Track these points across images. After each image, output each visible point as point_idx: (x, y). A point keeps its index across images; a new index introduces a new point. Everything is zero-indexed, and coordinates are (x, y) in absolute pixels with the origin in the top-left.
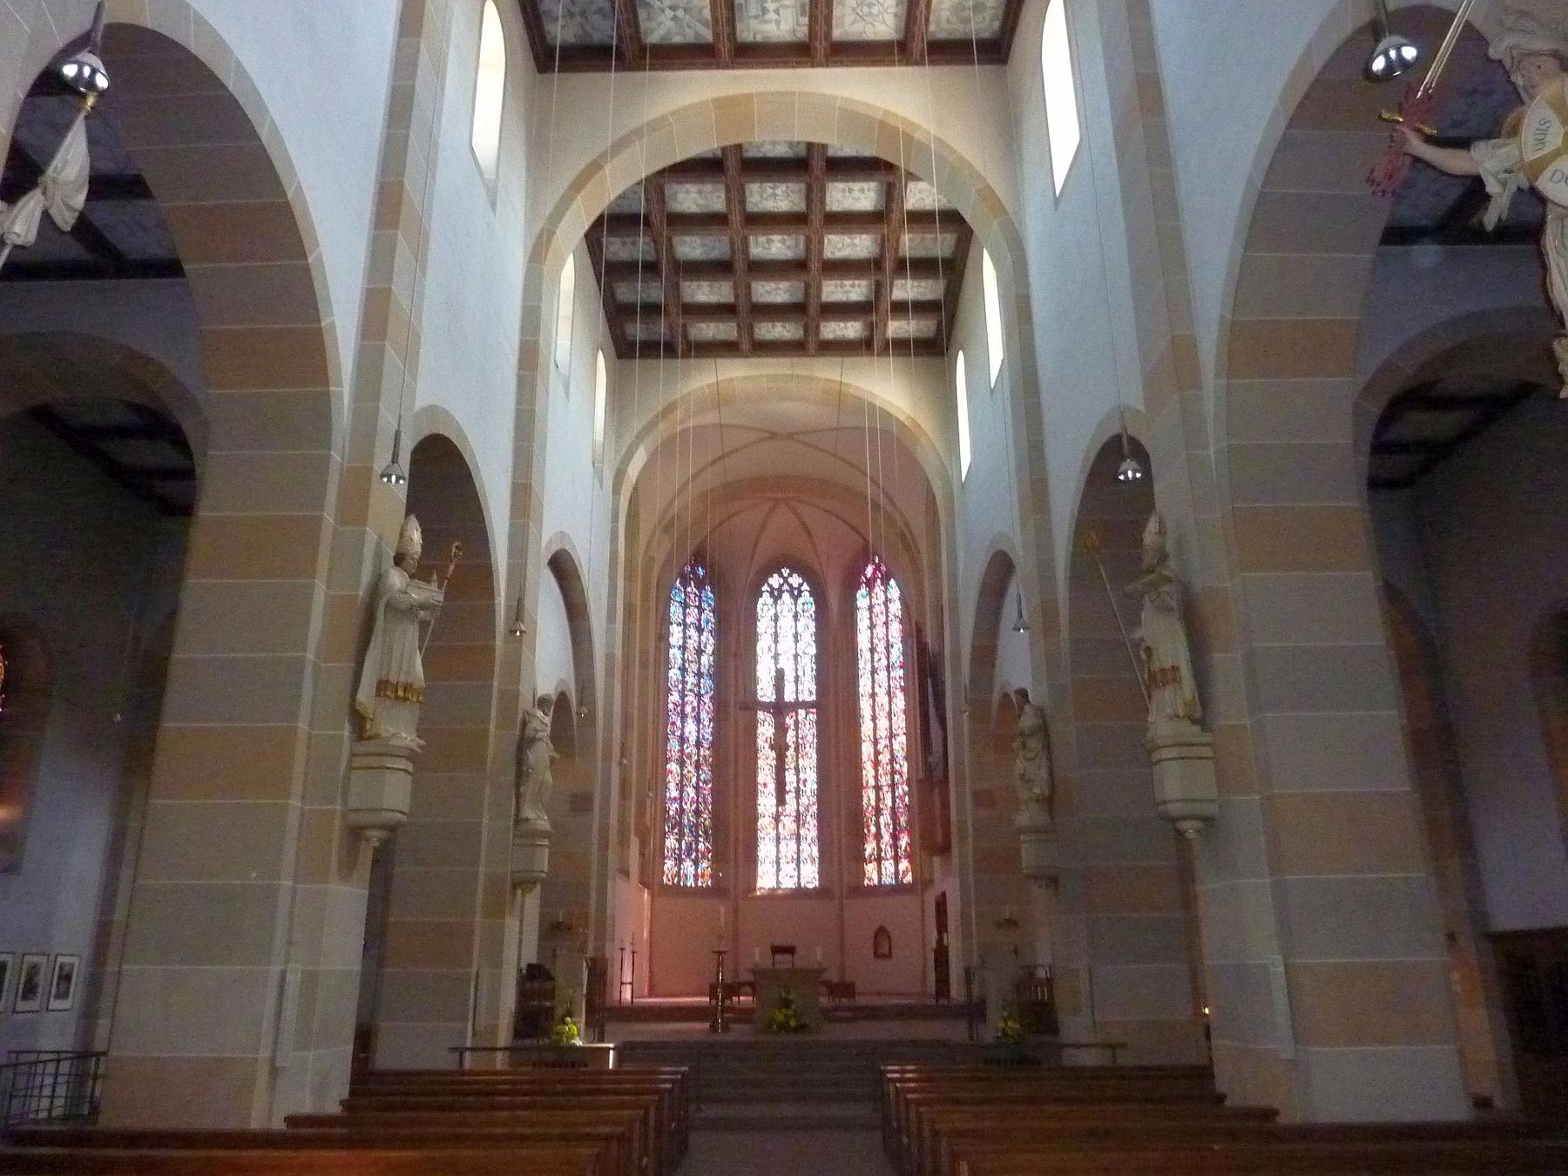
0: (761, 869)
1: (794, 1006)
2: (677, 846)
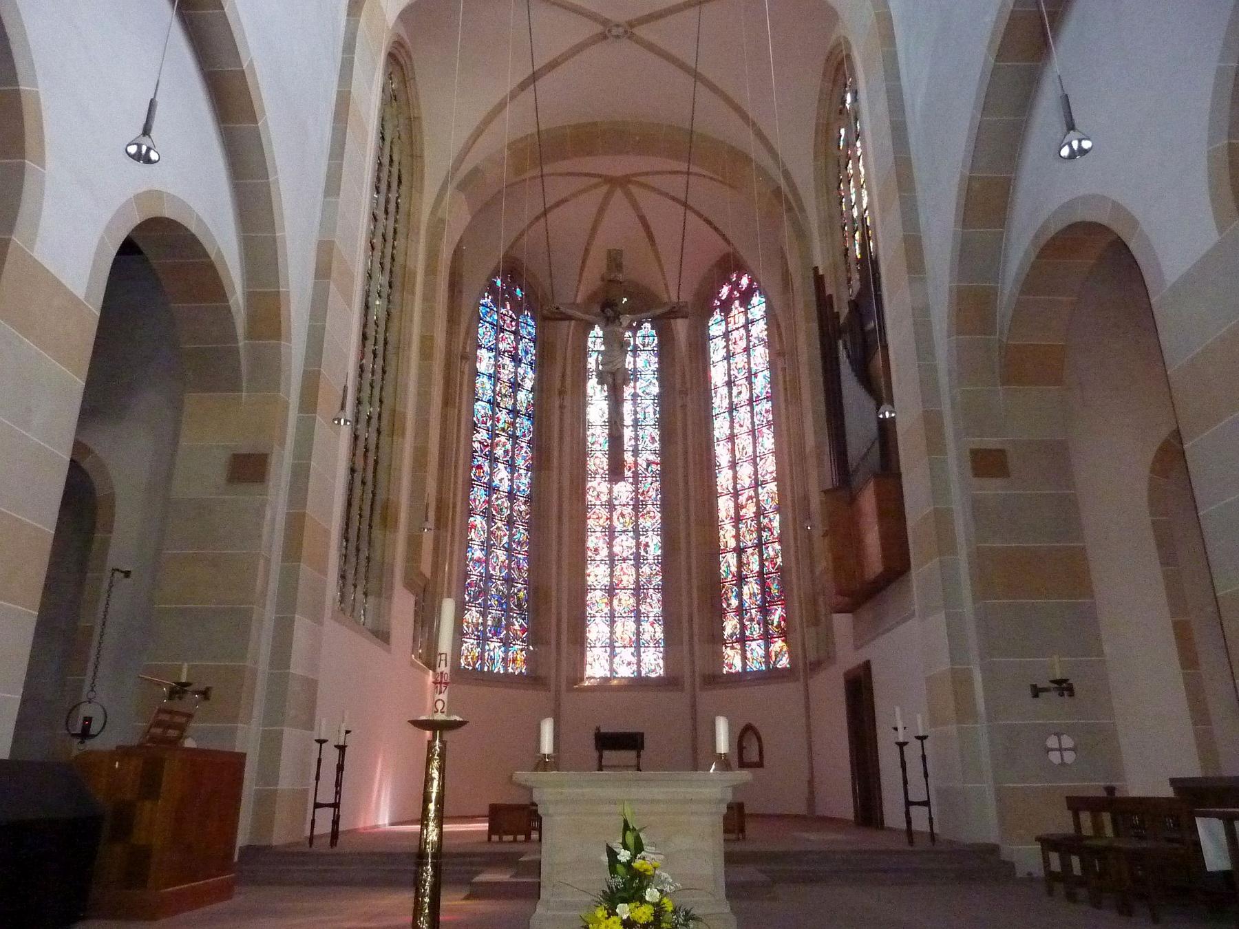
1: (651, 894)
2: (481, 621)
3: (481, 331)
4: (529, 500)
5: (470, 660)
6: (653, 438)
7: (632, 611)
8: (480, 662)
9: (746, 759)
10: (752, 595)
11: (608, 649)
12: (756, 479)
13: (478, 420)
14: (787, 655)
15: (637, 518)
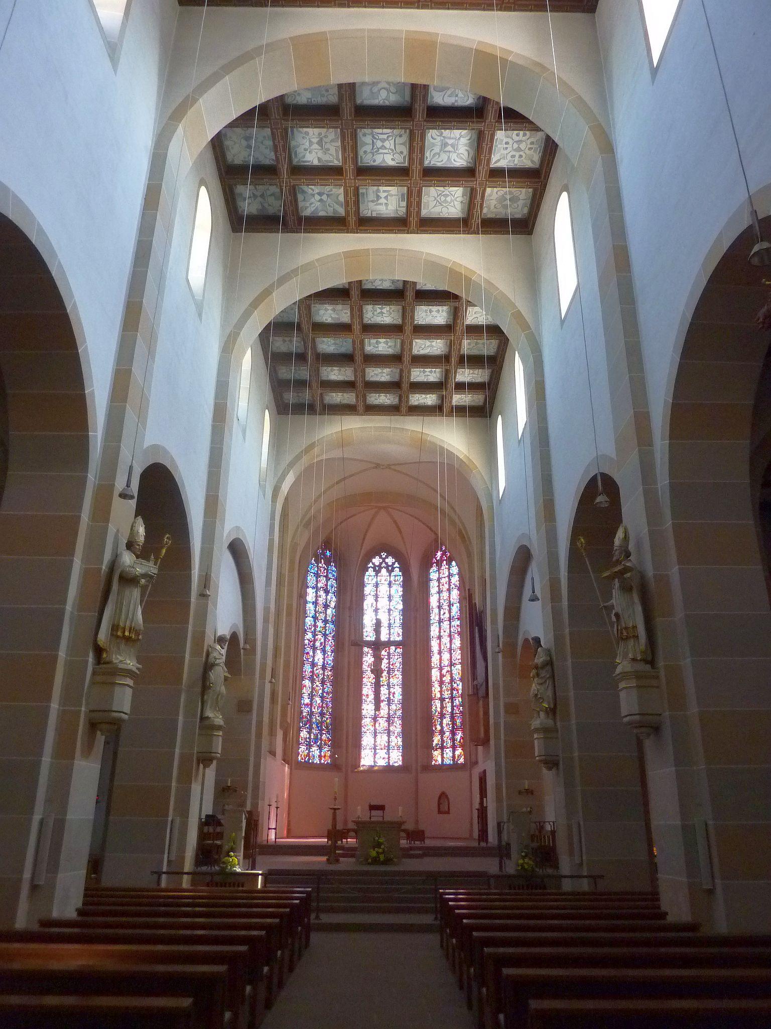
2: (308, 736)
3: (309, 578)
4: (333, 668)
5: (303, 757)
6: (399, 634)
7: (385, 730)
8: (307, 757)
9: (441, 810)
10: (448, 724)
11: (373, 750)
12: (451, 662)
13: (307, 628)
14: (463, 757)
15: (389, 678)
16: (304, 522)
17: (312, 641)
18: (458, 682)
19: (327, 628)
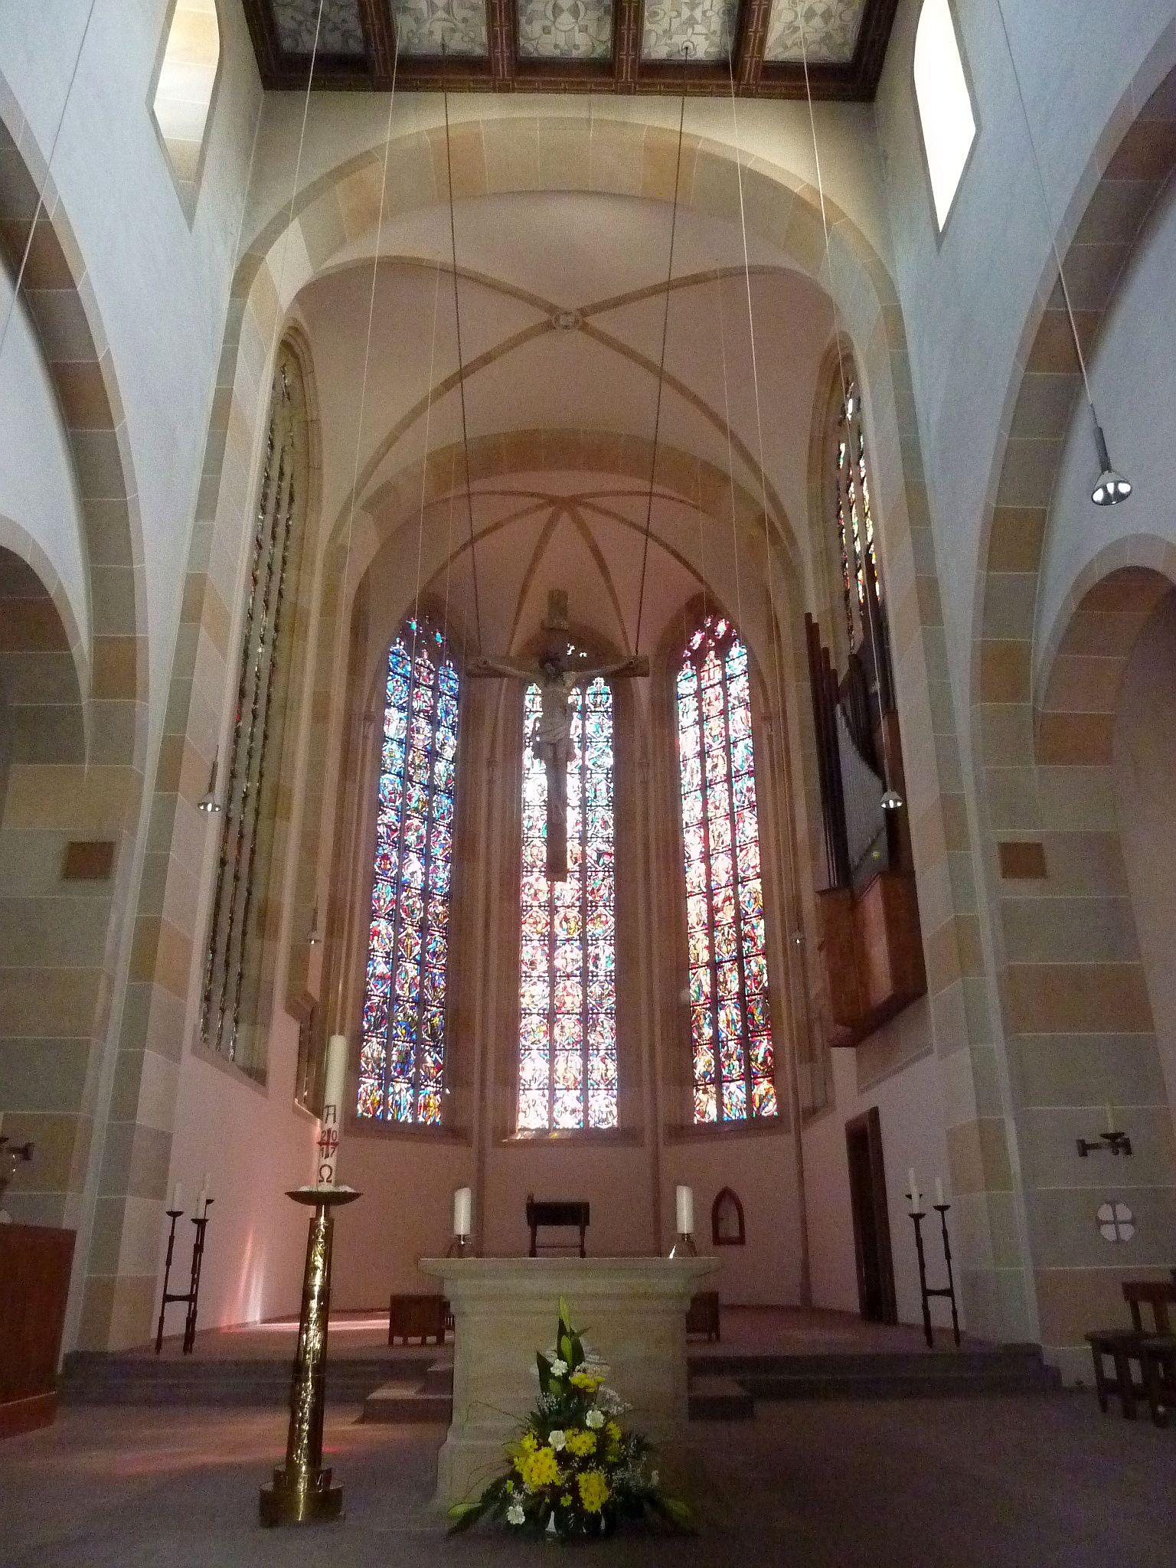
0: (523, 1100)
1: (594, 1418)
4: (448, 898)
6: (605, 822)
7: (578, 1042)
11: (546, 1092)
12: (735, 875)
13: (384, 797)
15: (585, 924)
16: (368, 492)
17: (396, 830)
18: (754, 921)
19: (434, 804)
